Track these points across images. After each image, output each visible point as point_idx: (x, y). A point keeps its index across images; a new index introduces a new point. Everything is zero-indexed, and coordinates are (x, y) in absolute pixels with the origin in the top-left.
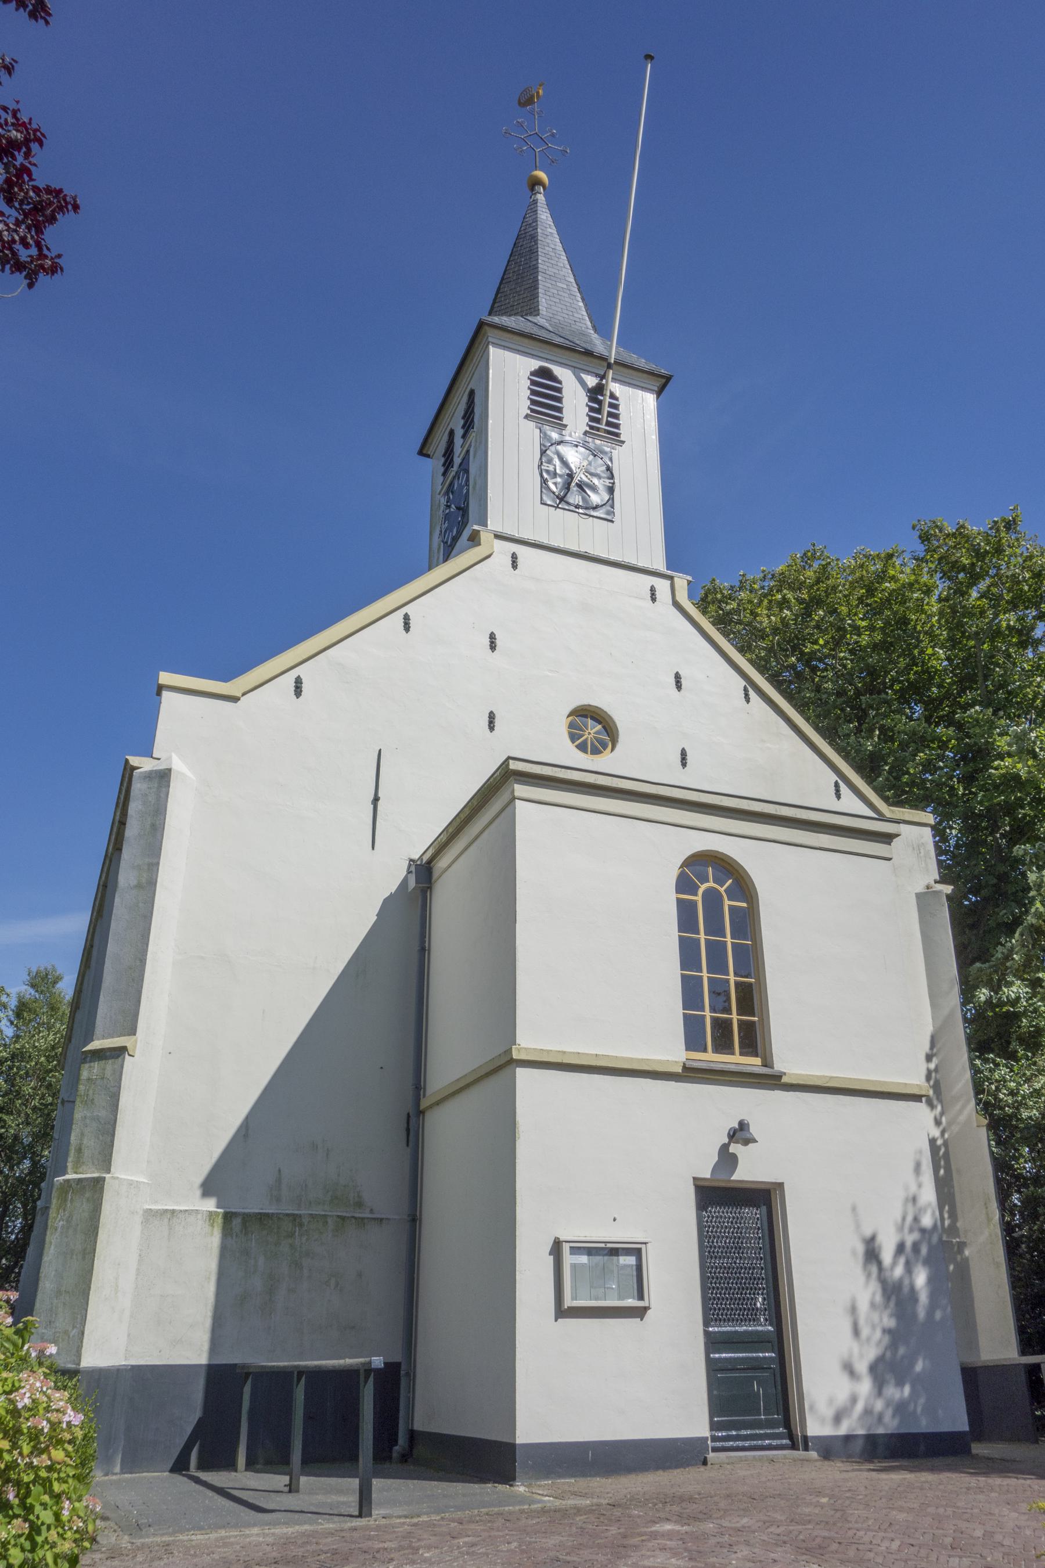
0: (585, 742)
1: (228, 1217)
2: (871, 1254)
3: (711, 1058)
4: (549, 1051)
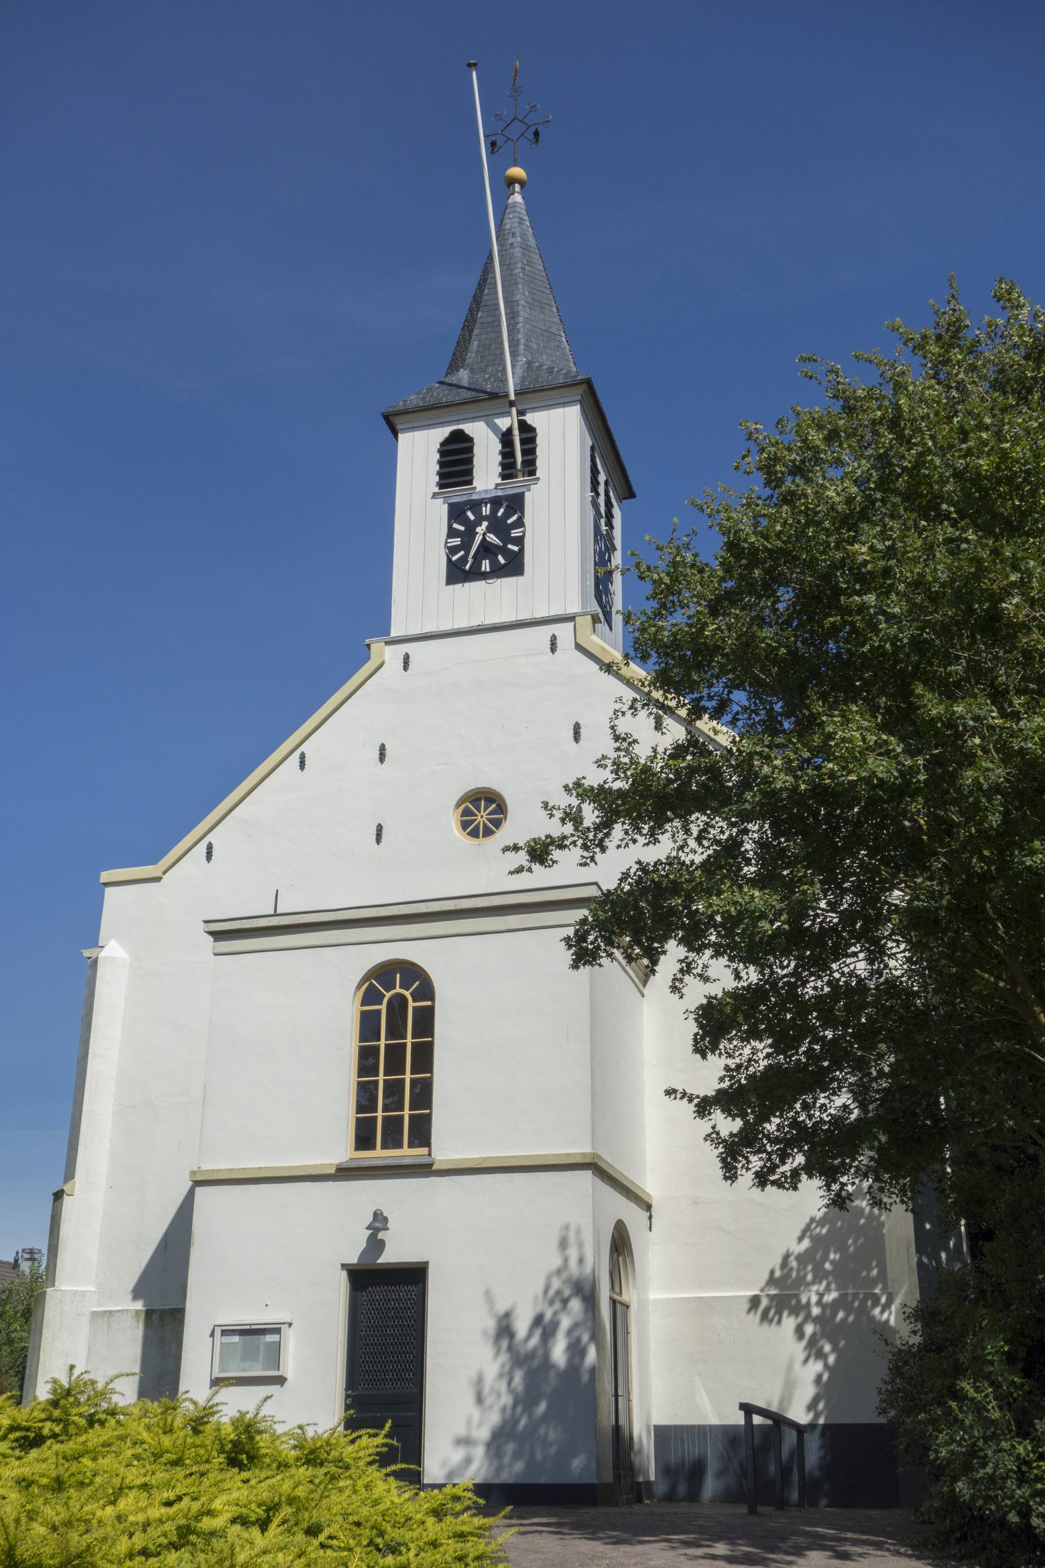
0: (477, 827)
1: (149, 1313)
2: (504, 1330)
3: (379, 1155)
4: (219, 1171)
